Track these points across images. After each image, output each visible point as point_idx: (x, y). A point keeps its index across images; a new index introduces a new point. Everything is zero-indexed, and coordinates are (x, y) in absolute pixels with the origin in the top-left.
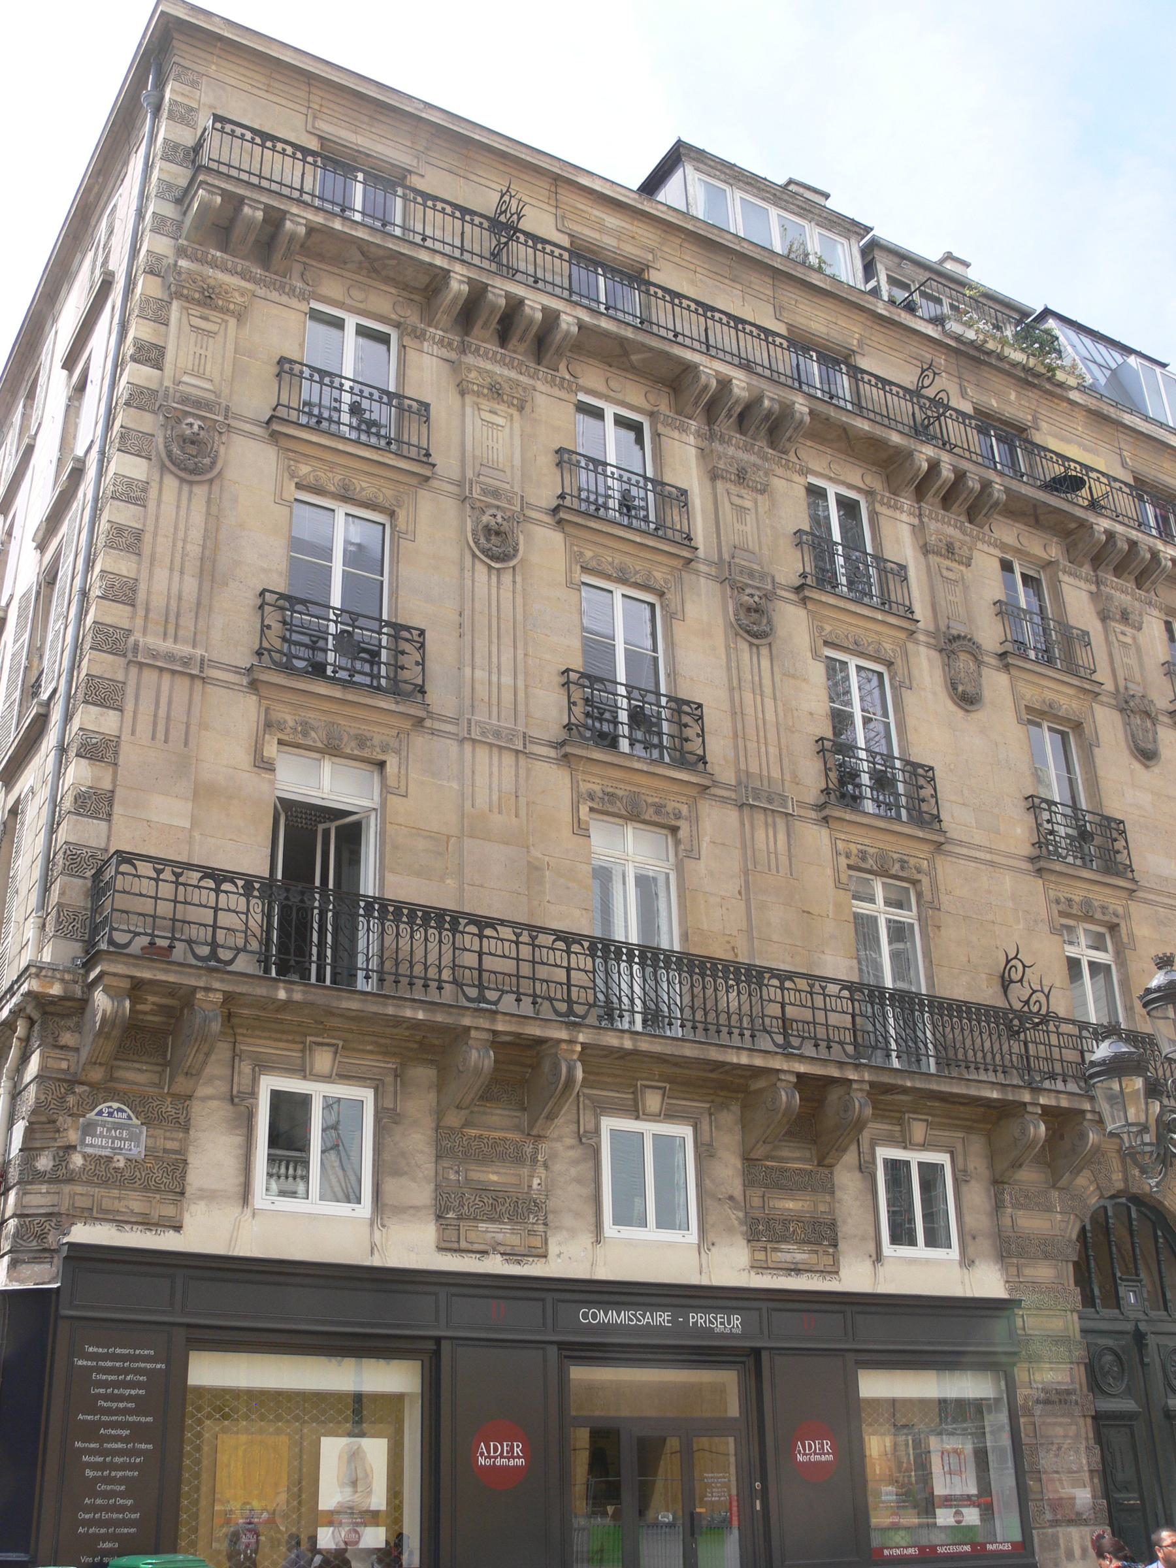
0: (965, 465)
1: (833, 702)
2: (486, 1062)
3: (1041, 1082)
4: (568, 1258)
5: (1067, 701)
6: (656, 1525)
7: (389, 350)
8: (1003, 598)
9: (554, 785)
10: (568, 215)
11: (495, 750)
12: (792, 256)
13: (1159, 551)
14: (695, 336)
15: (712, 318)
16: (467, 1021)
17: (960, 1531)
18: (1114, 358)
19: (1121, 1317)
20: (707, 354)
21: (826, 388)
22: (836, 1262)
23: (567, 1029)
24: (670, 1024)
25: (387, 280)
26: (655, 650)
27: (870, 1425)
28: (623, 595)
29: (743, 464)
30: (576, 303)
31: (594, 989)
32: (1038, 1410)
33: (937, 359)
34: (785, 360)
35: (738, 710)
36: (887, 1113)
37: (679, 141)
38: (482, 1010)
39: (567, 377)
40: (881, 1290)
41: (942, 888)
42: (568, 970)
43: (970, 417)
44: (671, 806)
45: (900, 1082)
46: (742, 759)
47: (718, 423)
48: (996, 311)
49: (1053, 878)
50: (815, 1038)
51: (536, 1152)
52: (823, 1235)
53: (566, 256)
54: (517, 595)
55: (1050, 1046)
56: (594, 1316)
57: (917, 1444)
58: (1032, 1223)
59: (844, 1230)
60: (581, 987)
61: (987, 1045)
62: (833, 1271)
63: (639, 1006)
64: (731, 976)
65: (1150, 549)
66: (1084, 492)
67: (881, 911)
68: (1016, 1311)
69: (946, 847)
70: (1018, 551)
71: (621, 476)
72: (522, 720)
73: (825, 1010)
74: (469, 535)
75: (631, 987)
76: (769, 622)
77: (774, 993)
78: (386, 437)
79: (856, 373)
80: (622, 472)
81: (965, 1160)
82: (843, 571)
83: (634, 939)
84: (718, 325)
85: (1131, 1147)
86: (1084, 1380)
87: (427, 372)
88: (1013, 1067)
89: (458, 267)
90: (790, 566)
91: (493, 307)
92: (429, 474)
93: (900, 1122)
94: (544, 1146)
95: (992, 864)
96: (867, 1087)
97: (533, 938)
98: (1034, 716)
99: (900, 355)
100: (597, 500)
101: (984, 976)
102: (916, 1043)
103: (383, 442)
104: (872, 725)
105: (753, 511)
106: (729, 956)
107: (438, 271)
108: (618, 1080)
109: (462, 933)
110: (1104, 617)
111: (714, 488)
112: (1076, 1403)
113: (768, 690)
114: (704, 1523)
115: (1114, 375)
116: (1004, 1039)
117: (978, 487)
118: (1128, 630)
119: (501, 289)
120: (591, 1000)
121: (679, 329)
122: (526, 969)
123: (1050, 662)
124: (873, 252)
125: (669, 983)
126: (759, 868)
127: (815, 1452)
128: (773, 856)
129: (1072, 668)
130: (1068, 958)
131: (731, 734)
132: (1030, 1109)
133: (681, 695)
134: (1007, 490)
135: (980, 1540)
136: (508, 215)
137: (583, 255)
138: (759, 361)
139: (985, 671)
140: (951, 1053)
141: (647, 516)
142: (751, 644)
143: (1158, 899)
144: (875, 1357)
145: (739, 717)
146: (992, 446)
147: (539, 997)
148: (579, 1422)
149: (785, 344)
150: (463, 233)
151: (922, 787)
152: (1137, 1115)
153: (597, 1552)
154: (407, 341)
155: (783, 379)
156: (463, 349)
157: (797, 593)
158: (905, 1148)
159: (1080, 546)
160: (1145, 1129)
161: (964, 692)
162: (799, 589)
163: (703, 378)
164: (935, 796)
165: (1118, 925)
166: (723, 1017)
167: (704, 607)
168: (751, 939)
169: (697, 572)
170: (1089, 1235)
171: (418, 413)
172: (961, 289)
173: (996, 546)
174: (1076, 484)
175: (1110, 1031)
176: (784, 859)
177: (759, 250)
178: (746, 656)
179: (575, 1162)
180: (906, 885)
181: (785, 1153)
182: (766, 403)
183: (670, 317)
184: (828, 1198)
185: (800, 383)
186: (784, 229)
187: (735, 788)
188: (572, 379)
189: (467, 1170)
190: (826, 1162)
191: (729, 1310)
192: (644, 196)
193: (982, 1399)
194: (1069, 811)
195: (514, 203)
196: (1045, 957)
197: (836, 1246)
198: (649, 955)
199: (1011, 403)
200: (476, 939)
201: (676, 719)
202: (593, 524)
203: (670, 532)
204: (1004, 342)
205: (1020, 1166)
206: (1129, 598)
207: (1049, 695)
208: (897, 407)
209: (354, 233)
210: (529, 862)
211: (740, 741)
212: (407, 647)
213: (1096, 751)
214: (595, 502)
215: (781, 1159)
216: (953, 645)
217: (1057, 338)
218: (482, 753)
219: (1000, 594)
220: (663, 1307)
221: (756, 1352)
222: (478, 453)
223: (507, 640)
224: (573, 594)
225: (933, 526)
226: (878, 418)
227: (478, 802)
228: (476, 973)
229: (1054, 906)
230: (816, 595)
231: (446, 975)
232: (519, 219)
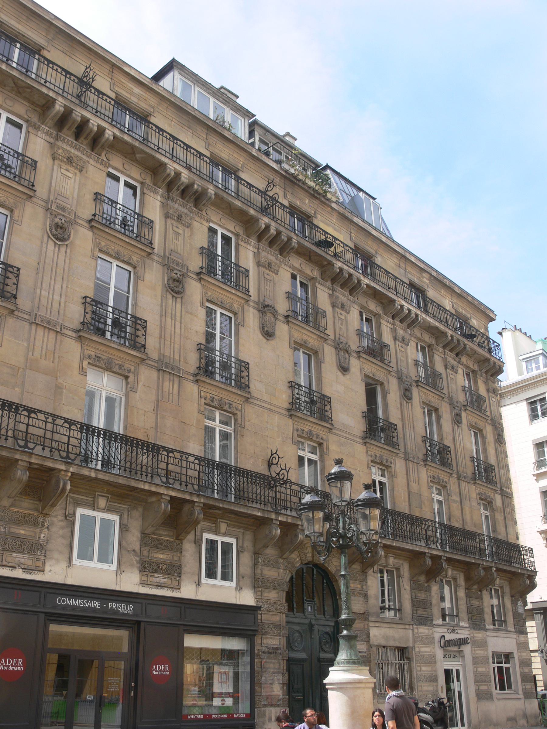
0: (281, 229)
1: (209, 328)
2: (25, 476)
3: (281, 510)
4: (54, 573)
5: (313, 341)
6: (85, 701)
7: (21, 132)
8: (290, 291)
9: (72, 350)
10: (116, 83)
11: (47, 330)
12: (217, 121)
13: (361, 280)
14: (167, 150)
15: (177, 143)
16: (17, 456)
17: (223, 709)
18: (353, 192)
19: (304, 617)
20: (171, 159)
21: (224, 184)
22: (179, 584)
23: (65, 465)
24: (114, 467)
25: (25, 98)
26: (128, 293)
27: (187, 659)
28: (117, 265)
29: (181, 213)
30: (114, 126)
31: (80, 447)
32: (263, 656)
33: (275, 179)
34: (207, 168)
35: (163, 326)
36: (210, 518)
37: (174, 59)
38: (26, 452)
39: (105, 159)
40: (199, 598)
41: (246, 418)
42: (69, 437)
43: (287, 208)
44: (126, 366)
45: (217, 504)
46: (162, 348)
47: (172, 192)
48: (305, 162)
49: (297, 419)
50: (181, 481)
51: (44, 522)
52: (175, 571)
53: (113, 102)
54: (67, 258)
55: (286, 494)
56: (64, 601)
57: (208, 669)
58: (270, 573)
59: (185, 569)
60: (74, 446)
61: (258, 491)
62: (178, 588)
63: (100, 458)
64: (145, 448)
65: (358, 278)
66: (332, 249)
67: (217, 425)
68: (258, 611)
69: (250, 400)
70: (300, 271)
71: (123, 210)
72: (61, 317)
73: (187, 468)
74: (48, 227)
75: (98, 448)
76: (183, 287)
77: (164, 458)
78: (14, 174)
79: (238, 179)
80: (124, 208)
81: (243, 542)
82: (220, 268)
83: (102, 426)
84: (179, 147)
85: (315, 542)
86: (285, 644)
87: (38, 146)
88: (269, 502)
89: (60, 99)
90: (196, 262)
91: (75, 121)
92: (32, 195)
93: (215, 522)
94: (48, 519)
95: (270, 410)
96: (202, 505)
97: (54, 420)
98: (297, 346)
99: (260, 175)
100: (110, 219)
101: (260, 460)
102: (226, 487)
103: (12, 176)
104: (224, 341)
105: (183, 235)
106: (146, 439)
107: (50, 99)
108: (87, 491)
109: (20, 414)
110: (334, 305)
111: (166, 222)
112: (281, 653)
113: (178, 319)
114: (106, 701)
115: (353, 199)
116: (266, 489)
117: (286, 239)
118: (343, 313)
119: (79, 113)
120: (78, 452)
121: (160, 146)
122: (48, 435)
123: (307, 322)
124: (254, 126)
125: (115, 448)
126: (164, 400)
127: (161, 670)
128: (171, 395)
129: (317, 326)
130: (299, 456)
131: (159, 337)
132: (274, 522)
133: (138, 315)
134: (299, 243)
135: (232, 712)
136: (88, 78)
137: (121, 104)
138: (195, 167)
139: (278, 323)
140: (242, 493)
141: (133, 230)
142: (173, 296)
143: (342, 434)
144: (195, 629)
145: (163, 329)
146: (294, 222)
147: (54, 448)
148: (52, 651)
149: (208, 161)
150: (65, 83)
151: (243, 372)
152: (319, 528)
153: (56, 713)
154: (30, 129)
155: (205, 177)
156: (57, 138)
157: (198, 276)
158: (216, 534)
159: (327, 273)
160: (321, 535)
161: (267, 331)
162: (198, 274)
163: (168, 171)
164: (248, 376)
165: (323, 443)
166: (139, 466)
167: (154, 276)
168: (156, 432)
169: (153, 259)
170: (294, 580)
171: (31, 165)
172: (291, 150)
173: (290, 267)
174: (329, 245)
175: (311, 490)
176: (176, 397)
177: (203, 116)
178: (170, 301)
179: (62, 528)
180: (230, 415)
181: (161, 532)
182: (196, 187)
183: (157, 140)
184: (179, 554)
185: (212, 180)
186: (215, 108)
187: (157, 362)
188: (107, 161)
189: (10, 527)
190: (180, 538)
191: (128, 603)
192: (153, 81)
193: (239, 650)
194: (307, 390)
195: (91, 73)
196: (289, 454)
197: (180, 577)
198: (108, 434)
199: (306, 204)
200: (27, 418)
201: (134, 326)
202: (107, 230)
203: (143, 239)
204: (306, 176)
205: (267, 547)
206: (345, 299)
207: (305, 337)
208: (255, 198)
209: (11, 72)
210: (56, 384)
211: (162, 340)
212: (10, 275)
213: (323, 365)
214: (110, 220)
215: (159, 535)
216: (265, 309)
217: (330, 179)
218: (40, 331)
219: (289, 289)
220: (97, 599)
221: (138, 623)
222: (57, 188)
223: (59, 278)
224: (93, 262)
225: (263, 254)
226: (246, 202)
227: (35, 353)
228: (24, 434)
229: (295, 432)
230: (206, 278)
231: (10, 433)
232: (93, 81)
